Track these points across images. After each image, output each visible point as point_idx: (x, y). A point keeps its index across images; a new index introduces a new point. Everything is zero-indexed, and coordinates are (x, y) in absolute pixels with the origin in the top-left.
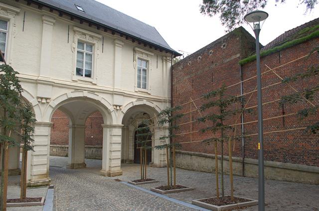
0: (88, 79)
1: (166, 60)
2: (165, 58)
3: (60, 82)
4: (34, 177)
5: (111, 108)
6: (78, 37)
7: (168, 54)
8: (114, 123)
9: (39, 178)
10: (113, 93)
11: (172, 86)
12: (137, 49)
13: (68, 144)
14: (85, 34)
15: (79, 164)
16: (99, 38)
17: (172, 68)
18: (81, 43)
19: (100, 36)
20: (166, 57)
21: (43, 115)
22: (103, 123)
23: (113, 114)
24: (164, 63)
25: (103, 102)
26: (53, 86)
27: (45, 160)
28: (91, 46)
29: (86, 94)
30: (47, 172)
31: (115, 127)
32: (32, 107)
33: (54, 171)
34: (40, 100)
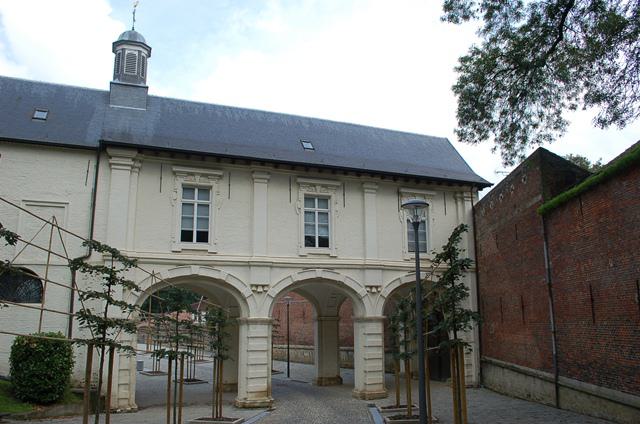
0: (323, 250)
1: (462, 199)
2: (458, 195)
3: (286, 261)
4: (250, 395)
5: (362, 291)
6: (304, 191)
7: (465, 188)
8: (369, 315)
9: (256, 397)
10: (364, 268)
11: (476, 242)
12: (403, 190)
13: (312, 344)
14: (192, 174)
15: (330, 379)
16: (338, 187)
17: (474, 210)
18: (309, 199)
19: (338, 184)
20: (462, 193)
21: (258, 309)
22: (353, 315)
23: (365, 300)
24: (459, 203)
25: (348, 283)
26: (271, 267)
27: (264, 371)
28: (324, 200)
29: (319, 273)
30: (268, 388)
31: (370, 320)
32: (274, 299)
33: (280, 389)
34: (254, 288)
